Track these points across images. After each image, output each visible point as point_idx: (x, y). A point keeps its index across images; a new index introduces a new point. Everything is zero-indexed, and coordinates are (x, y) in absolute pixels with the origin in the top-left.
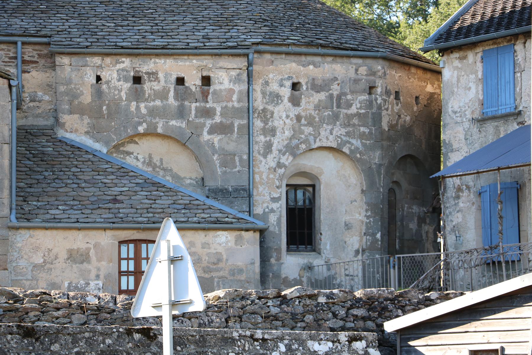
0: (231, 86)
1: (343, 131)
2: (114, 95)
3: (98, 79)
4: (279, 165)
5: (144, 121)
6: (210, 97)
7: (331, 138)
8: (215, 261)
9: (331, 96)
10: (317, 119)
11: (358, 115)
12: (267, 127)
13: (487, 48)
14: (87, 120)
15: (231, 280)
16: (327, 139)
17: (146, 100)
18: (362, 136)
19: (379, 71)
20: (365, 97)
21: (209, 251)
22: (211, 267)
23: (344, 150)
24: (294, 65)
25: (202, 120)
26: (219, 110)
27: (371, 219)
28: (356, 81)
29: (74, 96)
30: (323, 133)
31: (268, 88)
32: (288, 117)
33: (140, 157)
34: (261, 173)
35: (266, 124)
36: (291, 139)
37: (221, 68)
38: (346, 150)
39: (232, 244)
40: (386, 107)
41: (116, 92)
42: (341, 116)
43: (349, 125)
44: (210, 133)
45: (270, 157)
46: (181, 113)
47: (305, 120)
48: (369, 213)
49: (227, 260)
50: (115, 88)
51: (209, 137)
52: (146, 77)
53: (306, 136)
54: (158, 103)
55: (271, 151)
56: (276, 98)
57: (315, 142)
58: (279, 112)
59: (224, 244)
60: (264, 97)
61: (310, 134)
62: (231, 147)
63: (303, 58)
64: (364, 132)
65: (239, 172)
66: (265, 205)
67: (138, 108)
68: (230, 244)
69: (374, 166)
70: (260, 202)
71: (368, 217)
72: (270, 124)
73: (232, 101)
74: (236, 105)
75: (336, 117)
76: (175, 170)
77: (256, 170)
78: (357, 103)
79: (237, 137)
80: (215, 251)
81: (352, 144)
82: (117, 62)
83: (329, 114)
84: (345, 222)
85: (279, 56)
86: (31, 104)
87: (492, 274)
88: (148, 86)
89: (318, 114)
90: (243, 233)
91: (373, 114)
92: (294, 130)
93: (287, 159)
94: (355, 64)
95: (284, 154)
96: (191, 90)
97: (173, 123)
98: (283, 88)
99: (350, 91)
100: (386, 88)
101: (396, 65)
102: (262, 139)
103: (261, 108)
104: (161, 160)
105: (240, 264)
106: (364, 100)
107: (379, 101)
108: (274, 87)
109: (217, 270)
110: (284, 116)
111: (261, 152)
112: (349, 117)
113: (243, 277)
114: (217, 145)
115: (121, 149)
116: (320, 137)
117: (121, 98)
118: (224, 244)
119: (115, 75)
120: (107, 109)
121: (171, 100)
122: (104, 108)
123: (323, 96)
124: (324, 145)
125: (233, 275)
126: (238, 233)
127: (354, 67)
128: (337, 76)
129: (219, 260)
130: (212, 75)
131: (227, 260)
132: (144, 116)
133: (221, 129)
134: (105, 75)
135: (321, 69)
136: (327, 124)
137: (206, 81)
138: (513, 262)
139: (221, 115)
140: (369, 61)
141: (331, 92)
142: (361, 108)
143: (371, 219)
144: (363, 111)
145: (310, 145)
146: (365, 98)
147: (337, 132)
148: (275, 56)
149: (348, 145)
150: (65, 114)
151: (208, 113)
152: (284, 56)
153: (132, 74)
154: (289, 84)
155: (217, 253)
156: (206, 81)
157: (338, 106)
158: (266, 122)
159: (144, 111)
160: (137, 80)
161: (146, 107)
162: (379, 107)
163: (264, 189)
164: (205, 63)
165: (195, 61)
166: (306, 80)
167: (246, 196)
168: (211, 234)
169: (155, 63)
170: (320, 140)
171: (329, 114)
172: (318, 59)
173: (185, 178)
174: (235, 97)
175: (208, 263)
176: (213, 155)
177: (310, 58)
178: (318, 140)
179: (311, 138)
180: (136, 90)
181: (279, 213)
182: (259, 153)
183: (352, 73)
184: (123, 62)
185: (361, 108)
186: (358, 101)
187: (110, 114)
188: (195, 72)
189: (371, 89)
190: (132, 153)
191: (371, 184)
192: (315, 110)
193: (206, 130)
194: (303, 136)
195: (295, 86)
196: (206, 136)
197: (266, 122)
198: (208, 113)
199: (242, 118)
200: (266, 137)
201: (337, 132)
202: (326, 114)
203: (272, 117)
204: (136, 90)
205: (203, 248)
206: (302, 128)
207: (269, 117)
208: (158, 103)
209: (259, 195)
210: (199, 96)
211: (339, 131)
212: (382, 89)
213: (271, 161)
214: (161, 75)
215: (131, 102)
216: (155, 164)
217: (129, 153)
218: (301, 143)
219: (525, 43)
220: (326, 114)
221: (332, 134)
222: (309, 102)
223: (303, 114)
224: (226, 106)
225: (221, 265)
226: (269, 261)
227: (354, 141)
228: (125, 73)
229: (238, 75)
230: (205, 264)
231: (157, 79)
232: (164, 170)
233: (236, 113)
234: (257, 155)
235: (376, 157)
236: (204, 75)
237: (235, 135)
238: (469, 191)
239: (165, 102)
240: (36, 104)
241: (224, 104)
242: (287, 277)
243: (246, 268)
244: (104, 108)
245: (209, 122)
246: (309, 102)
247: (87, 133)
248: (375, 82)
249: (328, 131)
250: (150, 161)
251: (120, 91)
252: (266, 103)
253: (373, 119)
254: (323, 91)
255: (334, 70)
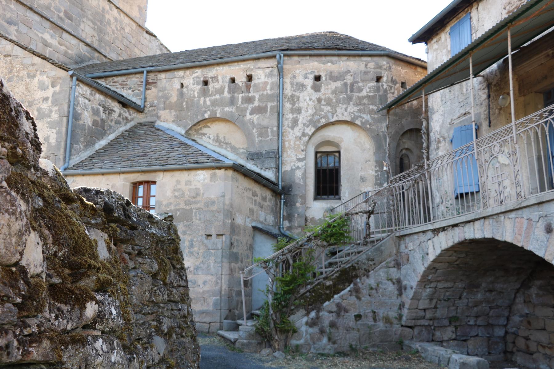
0: (266, 80)
1: (356, 109)
2: (191, 94)
3: (182, 85)
4: (304, 134)
5: (209, 110)
6: (251, 89)
7: (346, 114)
8: (195, 195)
9: (345, 84)
10: (334, 101)
11: (368, 97)
12: (294, 107)
13: (453, 25)
14: (174, 113)
15: (206, 211)
16: (343, 114)
17: (210, 96)
18: (371, 112)
19: (384, 65)
20: (374, 84)
21: (190, 187)
22: (192, 200)
23: (356, 122)
24: (316, 63)
25: (246, 105)
26: (257, 97)
27: (379, 173)
28: (366, 73)
29: (166, 98)
30: (339, 110)
31: (295, 80)
32: (310, 100)
33: (211, 136)
34: (289, 141)
35: (293, 105)
36: (313, 115)
37: (259, 68)
38: (358, 122)
39: (207, 181)
40: (392, 91)
41: (192, 93)
42: (354, 98)
43: (360, 105)
44: (251, 113)
45: (296, 129)
46: (232, 102)
47: (325, 101)
48: (377, 169)
49: (203, 194)
50: (191, 90)
51: (251, 117)
52: (210, 80)
53: (325, 113)
54: (218, 96)
55: (297, 125)
56: (301, 87)
57: (333, 117)
58: (304, 96)
59: (202, 181)
60: (292, 87)
61: (328, 111)
62: (265, 122)
63: (323, 58)
64: (373, 109)
65: (270, 140)
66: (292, 164)
67: (205, 101)
68: (206, 181)
69: (381, 134)
70: (289, 162)
71: (376, 172)
72: (297, 105)
73: (267, 90)
74: (269, 92)
75: (350, 99)
76: (233, 144)
77: (286, 139)
78: (368, 88)
79: (270, 115)
80: (194, 187)
81: (363, 118)
82: (194, 73)
83: (344, 97)
84: (361, 177)
85: (304, 58)
86: (150, 109)
87: (460, 206)
88: (211, 86)
89: (334, 97)
90: (217, 171)
91: (380, 96)
92: (315, 109)
93: (310, 130)
94: (365, 61)
95: (307, 127)
96: (239, 85)
97: (227, 109)
98: (307, 80)
99: (361, 80)
100: (392, 78)
101: (402, 63)
102: (290, 116)
103: (290, 94)
104: (224, 137)
105: (213, 197)
106: (373, 86)
107: (385, 87)
108: (300, 79)
109: (196, 203)
110: (308, 99)
111: (290, 126)
112: (361, 99)
113: (214, 208)
114: (256, 122)
115: (200, 132)
116: (337, 114)
117: (194, 96)
118: (202, 181)
119: (191, 81)
120: (186, 104)
121: (226, 94)
122: (184, 103)
123: (339, 84)
124: (340, 119)
125: (208, 206)
126: (213, 171)
127: (364, 63)
128: (350, 70)
129: (198, 194)
130: (253, 74)
131: (203, 194)
132: (208, 106)
133: (259, 110)
134: (185, 82)
135: (337, 65)
136: (343, 104)
137: (250, 78)
138: (472, 193)
139: (259, 100)
140: (376, 59)
141: (345, 81)
142: (370, 92)
143: (379, 173)
144: (372, 94)
145: (328, 119)
146: (373, 84)
147: (351, 109)
148: (301, 58)
149: (359, 119)
150: (160, 110)
151: (250, 100)
152: (308, 58)
153: (202, 79)
154: (311, 77)
155: (196, 188)
156: (250, 78)
157: (352, 91)
158: (293, 105)
159: (208, 103)
160: (206, 83)
161: (210, 100)
162: (385, 91)
163: (292, 152)
164: (248, 66)
165: (242, 66)
166: (325, 73)
167: (273, 156)
168: (193, 173)
169: (216, 70)
170: (337, 116)
171: (344, 97)
172: (335, 59)
173: (239, 148)
174: (268, 87)
175: (189, 197)
176: (253, 129)
177: (328, 58)
178: (335, 116)
179: (330, 115)
180: (204, 89)
181: (303, 170)
182: (288, 127)
183: (362, 67)
184: (197, 72)
185: (370, 92)
186: (367, 87)
187: (187, 108)
188: (242, 73)
189: (378, 79)
190: (206, 134)
191: (379, 148)
192: (333, 94)
193: (248, 112)
194: (323, 113)
195: (318, 78)
196: (248, 117)
197: (293, 105)
198: (250, 100)
199: (273, 101)
200: (293, 114)
201: (351, 109)
202: (342, 96)
203: (298, 100)
204: (204, 89)
205: (186, 185)
206: (322, 107)
207: (295, 100)
208: (218, 96)
209: (288, 156)
210: (244, 89)
211: (352, 108)
212: (387, 78)
213: (297, 132)
214: (220, 78)
215: (200, 98)
216: (221, 140)
217: (204, 134)
218: (321, 118)
219: (477, 8)
220: (342, 96)
221: (346, 111)
222: (327, 89)
223: (323, 97)
224: (262, 94)
225: (199, 198)
226: (295, 205)
227: (364, 116)
228: (198, 79)
229: (271, 72)
230: (187, 198)
231: (217, 81)
232: (226, 144)
233: (270, 98)
234: (287, 128)
235: (383, 127)
236: (248, 74)
237: (268, 113)
238: (445, 141)
239: (222, 96)
240: (153, 108)
241: (261, 93)
242: (313, 218)
243: (218, 200)
244: (184, 103)
245: (250, 106)
246: (327, 89)
247: (173, 121)
248: (381, 73)
249: (343, 109)
250: (218, 138)
251: (194, 91)
252: (294, 91)
253: (380, 100)
254: (338, 80)
255: (348, 66)
